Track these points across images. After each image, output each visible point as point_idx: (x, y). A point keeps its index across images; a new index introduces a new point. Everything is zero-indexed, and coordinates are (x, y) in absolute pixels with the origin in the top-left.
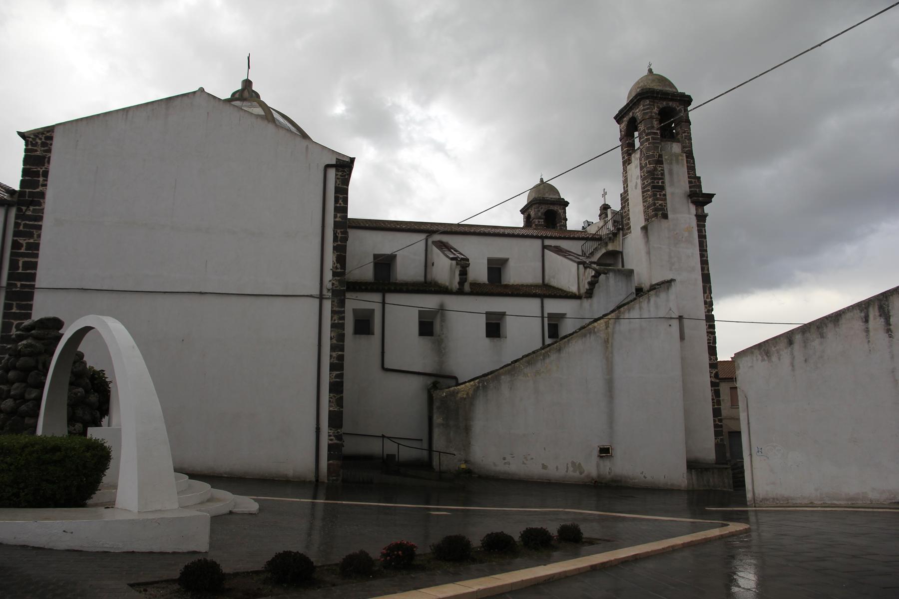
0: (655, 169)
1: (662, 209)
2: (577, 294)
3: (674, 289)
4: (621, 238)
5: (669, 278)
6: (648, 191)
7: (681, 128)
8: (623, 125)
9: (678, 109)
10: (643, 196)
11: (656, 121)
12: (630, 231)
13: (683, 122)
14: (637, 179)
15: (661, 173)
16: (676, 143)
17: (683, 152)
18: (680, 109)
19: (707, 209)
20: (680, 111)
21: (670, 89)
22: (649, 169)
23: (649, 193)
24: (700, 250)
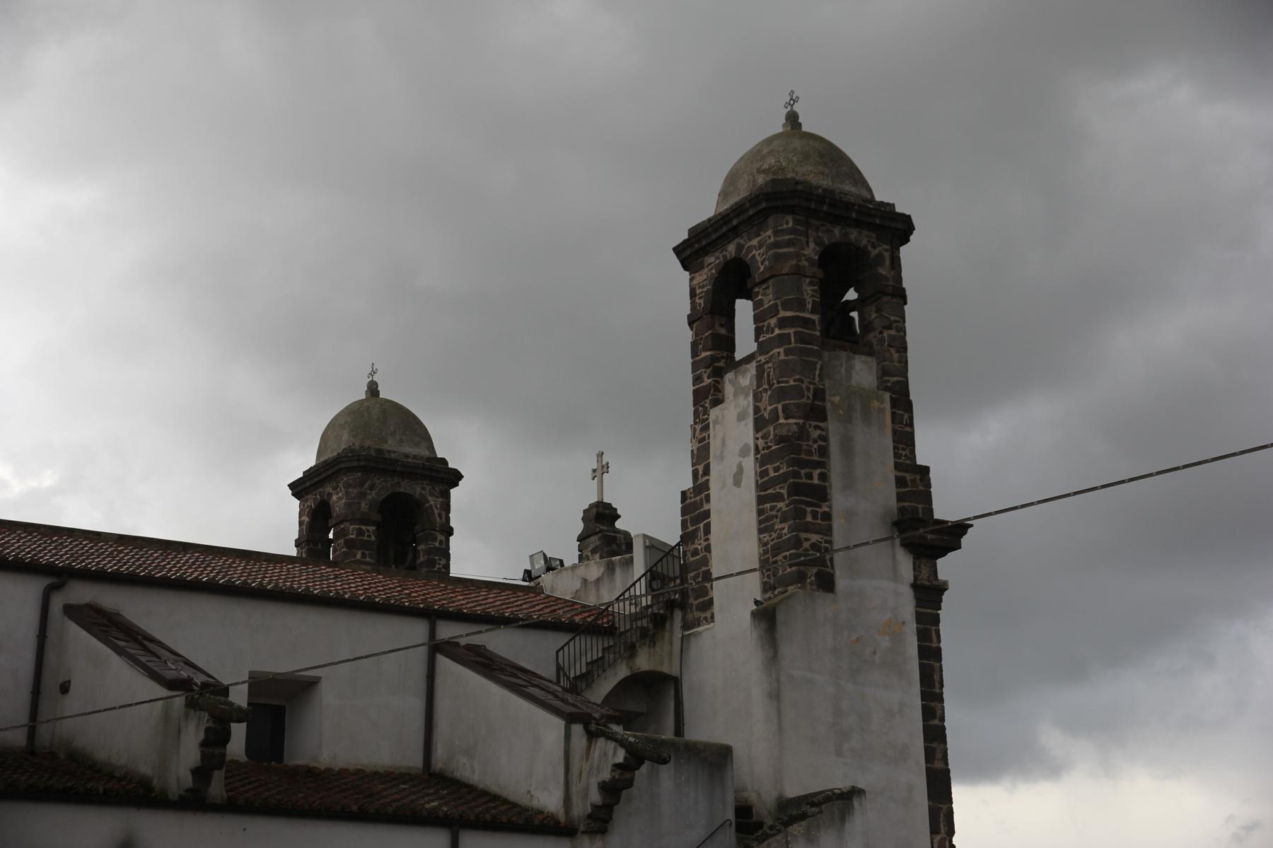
0: (802, 434)
1: (820, 562)
2: (562, 818)
3: (863, 818)
4: (678, 634)
5: (840, 783)
6: (778, 497)
7: (878, 310)
8: (701, 277)
9: (874, 252)
10: (760, 512)
11: (811, 284)
12: (708, 615)
13: (886, 294)
14: (744, 452)
15: (820, 447)
16: (863, 358)
17: (883, 386)
18: (880, 255)
19: (946, 566)
20: (879, 259)
21: (853, 189)
22: (784, 432)
23: (780, 505)
24: (924, 696)
